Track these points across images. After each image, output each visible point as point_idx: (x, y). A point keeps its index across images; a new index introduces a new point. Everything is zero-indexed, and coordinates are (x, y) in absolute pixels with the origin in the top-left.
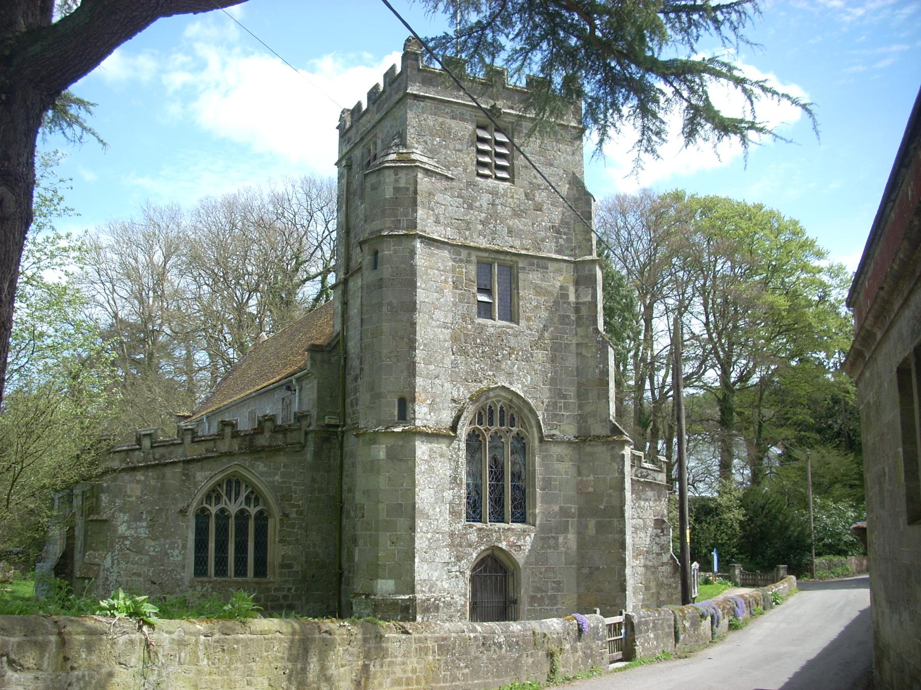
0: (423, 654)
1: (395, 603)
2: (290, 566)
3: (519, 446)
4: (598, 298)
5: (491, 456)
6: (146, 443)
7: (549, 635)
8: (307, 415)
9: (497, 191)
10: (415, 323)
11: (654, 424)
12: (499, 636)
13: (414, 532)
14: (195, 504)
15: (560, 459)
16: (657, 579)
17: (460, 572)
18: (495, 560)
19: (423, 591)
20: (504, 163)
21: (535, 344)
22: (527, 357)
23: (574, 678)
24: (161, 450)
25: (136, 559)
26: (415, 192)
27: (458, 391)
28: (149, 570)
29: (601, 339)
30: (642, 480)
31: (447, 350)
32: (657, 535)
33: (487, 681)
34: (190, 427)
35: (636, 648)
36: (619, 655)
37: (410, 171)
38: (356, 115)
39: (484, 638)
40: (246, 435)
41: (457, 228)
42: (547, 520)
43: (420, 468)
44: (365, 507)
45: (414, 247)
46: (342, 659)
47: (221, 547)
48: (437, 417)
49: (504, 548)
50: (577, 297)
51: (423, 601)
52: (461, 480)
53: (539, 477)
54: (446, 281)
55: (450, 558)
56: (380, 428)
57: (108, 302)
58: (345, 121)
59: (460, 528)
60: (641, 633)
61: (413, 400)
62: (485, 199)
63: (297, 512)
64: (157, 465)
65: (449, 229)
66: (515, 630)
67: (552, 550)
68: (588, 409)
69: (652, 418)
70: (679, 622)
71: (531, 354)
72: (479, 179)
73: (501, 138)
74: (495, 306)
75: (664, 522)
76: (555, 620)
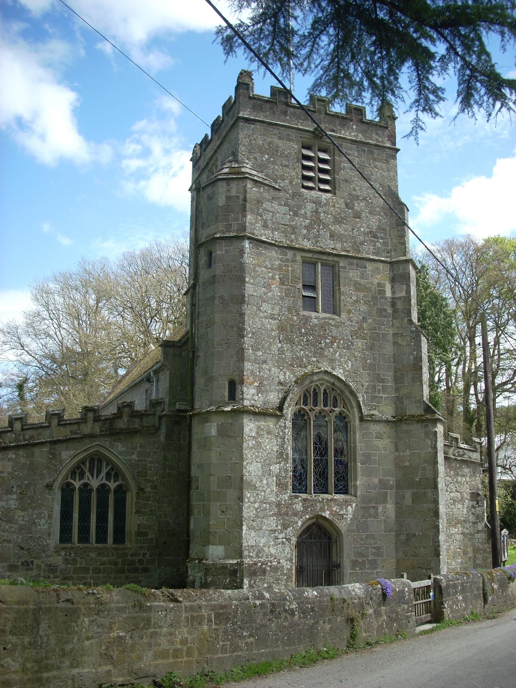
0: (195, 623)
1: (224, 567)
2: (145, 534)
3: (342, 425)
4: (412, 293)
5: (316, 433)
6: (18, 426)
7: (348, 601)
8: (161, 402)
9: (320, 201)
10: (244, 314)
11: (478, 421)
12: (291, 603)
13: (242, 502)
14: (60, 479)
15: (379, 437)
16: (473, 545)
17: (286, 539)
18: (319, 527)
19: (250, 557)
20: (327, 177)
21: (355, 334)
22: (348, 345)
23: (377, 642)
24: (31, 432)
25: (7, 527)
26: (245, 200)
27: (285, 375)
28: (18, 538)
29: (414, 329)
30: (459, 458)
31: (274, 338)
32: (473, 507)
33: (275, 649)
34: (56, 412)
35: (444, 610)
36: (428, 617)
37: (240, 182)
38: (204, 146)
39: (273, 605)
40: (106, 419)
41: (283, 232)
42: (367, 492)
43: (248, 443)
44: (199, 480)
45: (243, 247)
46: (87, 631)
47: (84, 517)
48: (264, 398)
49: (327, 517)
50: (393, 293)
51: (250, 566)
52: (287, 455)
53: (359, 452)
54: (273, 278)
55: (277, 526)
56: (212, 407)
57: (56, 334)
58: (197, 154)
59: (287, 498)
60: (449, 595)
61: (242, 382)
62: (310, 206)
63: (151, 486)
64: (26, 445)
65: (277, 233)
66: (310, 595)
67: (372, 519)
68: (404, 391)
69: (476, 416)
70: (487, 585)
71: (352, 343)
72: (303, 190)
73: (323, 156)
74: (318, 300)
75: (478, 495)
76: (357, 585)
